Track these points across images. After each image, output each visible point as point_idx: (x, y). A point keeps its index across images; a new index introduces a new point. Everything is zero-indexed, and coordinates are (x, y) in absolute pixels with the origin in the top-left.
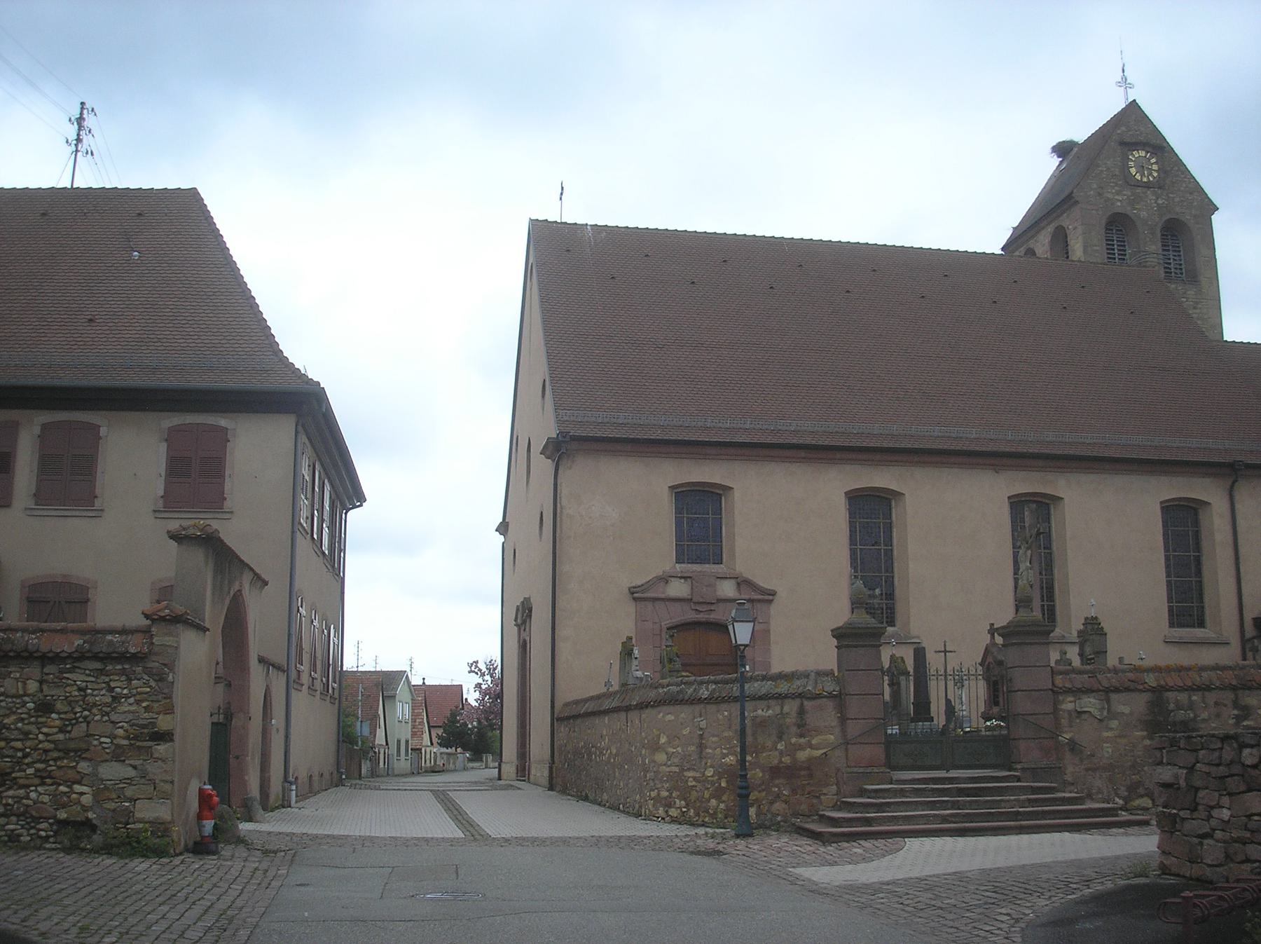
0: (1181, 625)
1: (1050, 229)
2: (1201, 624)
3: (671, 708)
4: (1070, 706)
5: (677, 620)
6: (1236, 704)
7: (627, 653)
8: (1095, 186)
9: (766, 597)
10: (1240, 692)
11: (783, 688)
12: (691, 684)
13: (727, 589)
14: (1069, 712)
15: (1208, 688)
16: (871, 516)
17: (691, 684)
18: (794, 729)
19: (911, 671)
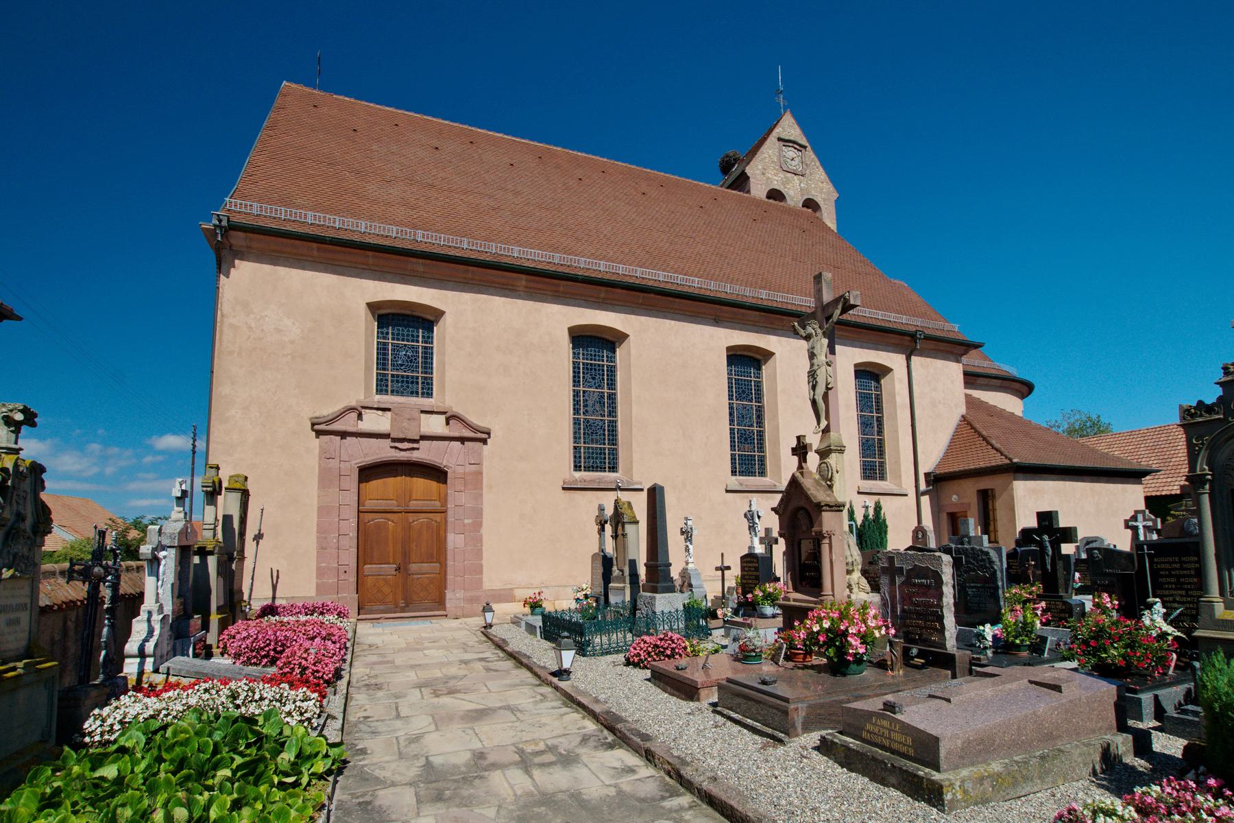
13: (435, 425)
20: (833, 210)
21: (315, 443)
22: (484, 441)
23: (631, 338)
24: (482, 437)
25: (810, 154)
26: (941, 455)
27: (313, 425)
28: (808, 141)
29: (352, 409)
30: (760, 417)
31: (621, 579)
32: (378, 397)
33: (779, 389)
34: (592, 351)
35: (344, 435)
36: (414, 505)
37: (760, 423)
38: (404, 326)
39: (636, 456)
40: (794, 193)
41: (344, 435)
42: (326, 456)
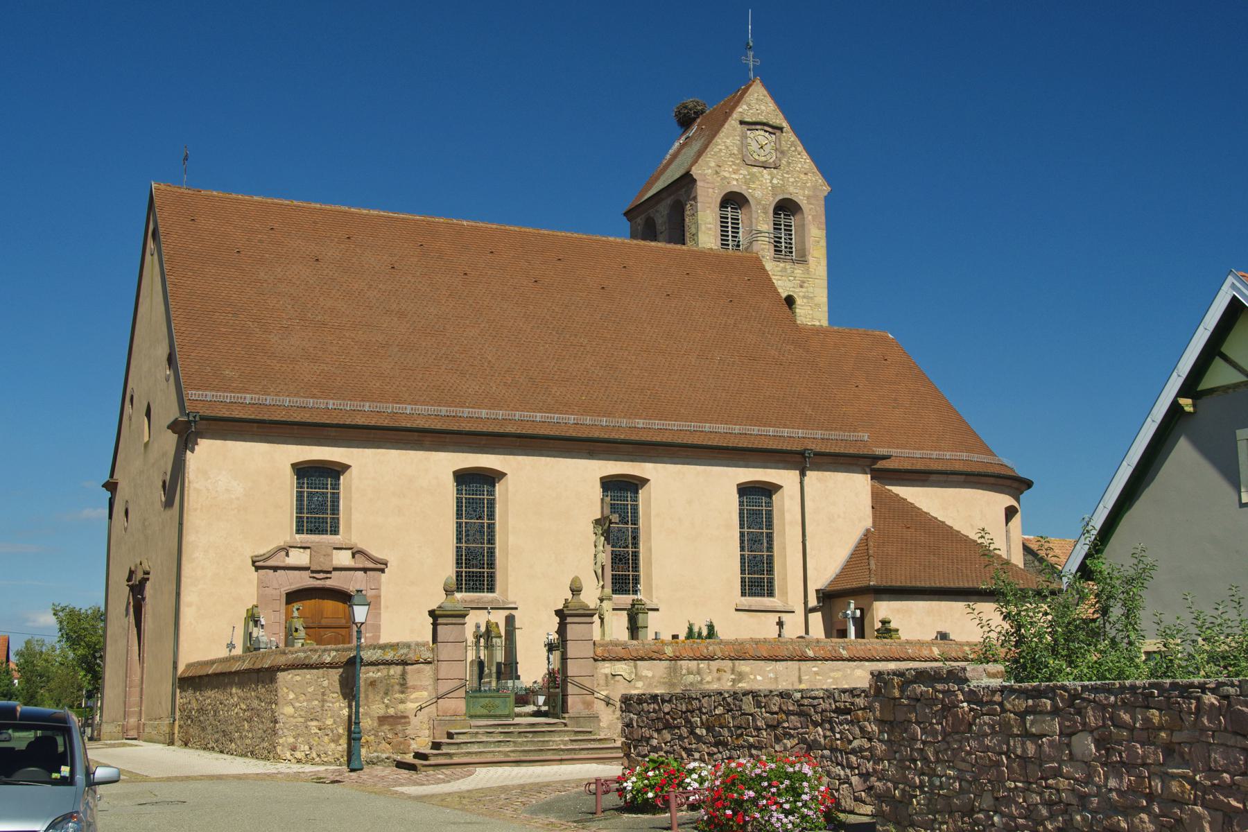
0: (752, 594)
1: (669, 201)
2: (771, 594)
3: (297, 671)
4: (607, 671)
5: (295, 587)
6: (733, 671)
7: (253, 618)
8: (713, 164)
9: (379, 566)
10: (737, 662)
11: (389, 656)
12: (316, 651)
13: (344, 559)
14: (606, 676)
15: (712, 659)
16: (476, 489)
17: (316, 651)
18: (397, 688)
19: (503, 633)
20: (821, 210)
21: (254, 575)
22: (383, 571)
23: (509, 476)
24: (380, 567)
25: (789, 136)
26: (838, 570)
27: (254, 562)
28: (787, 118)
29: (283, 549)
30: (635, 538)
31: (490, 675)
32: (298, 536)
33: (653, 513)
34: (474, 486)
35: (275, 569)
36: (324, 622)
37: (635, 544)
38: (318, 481)
39: (511, 579)
40: (763, 190)
41: (275, 569)
42: (262, 585)
